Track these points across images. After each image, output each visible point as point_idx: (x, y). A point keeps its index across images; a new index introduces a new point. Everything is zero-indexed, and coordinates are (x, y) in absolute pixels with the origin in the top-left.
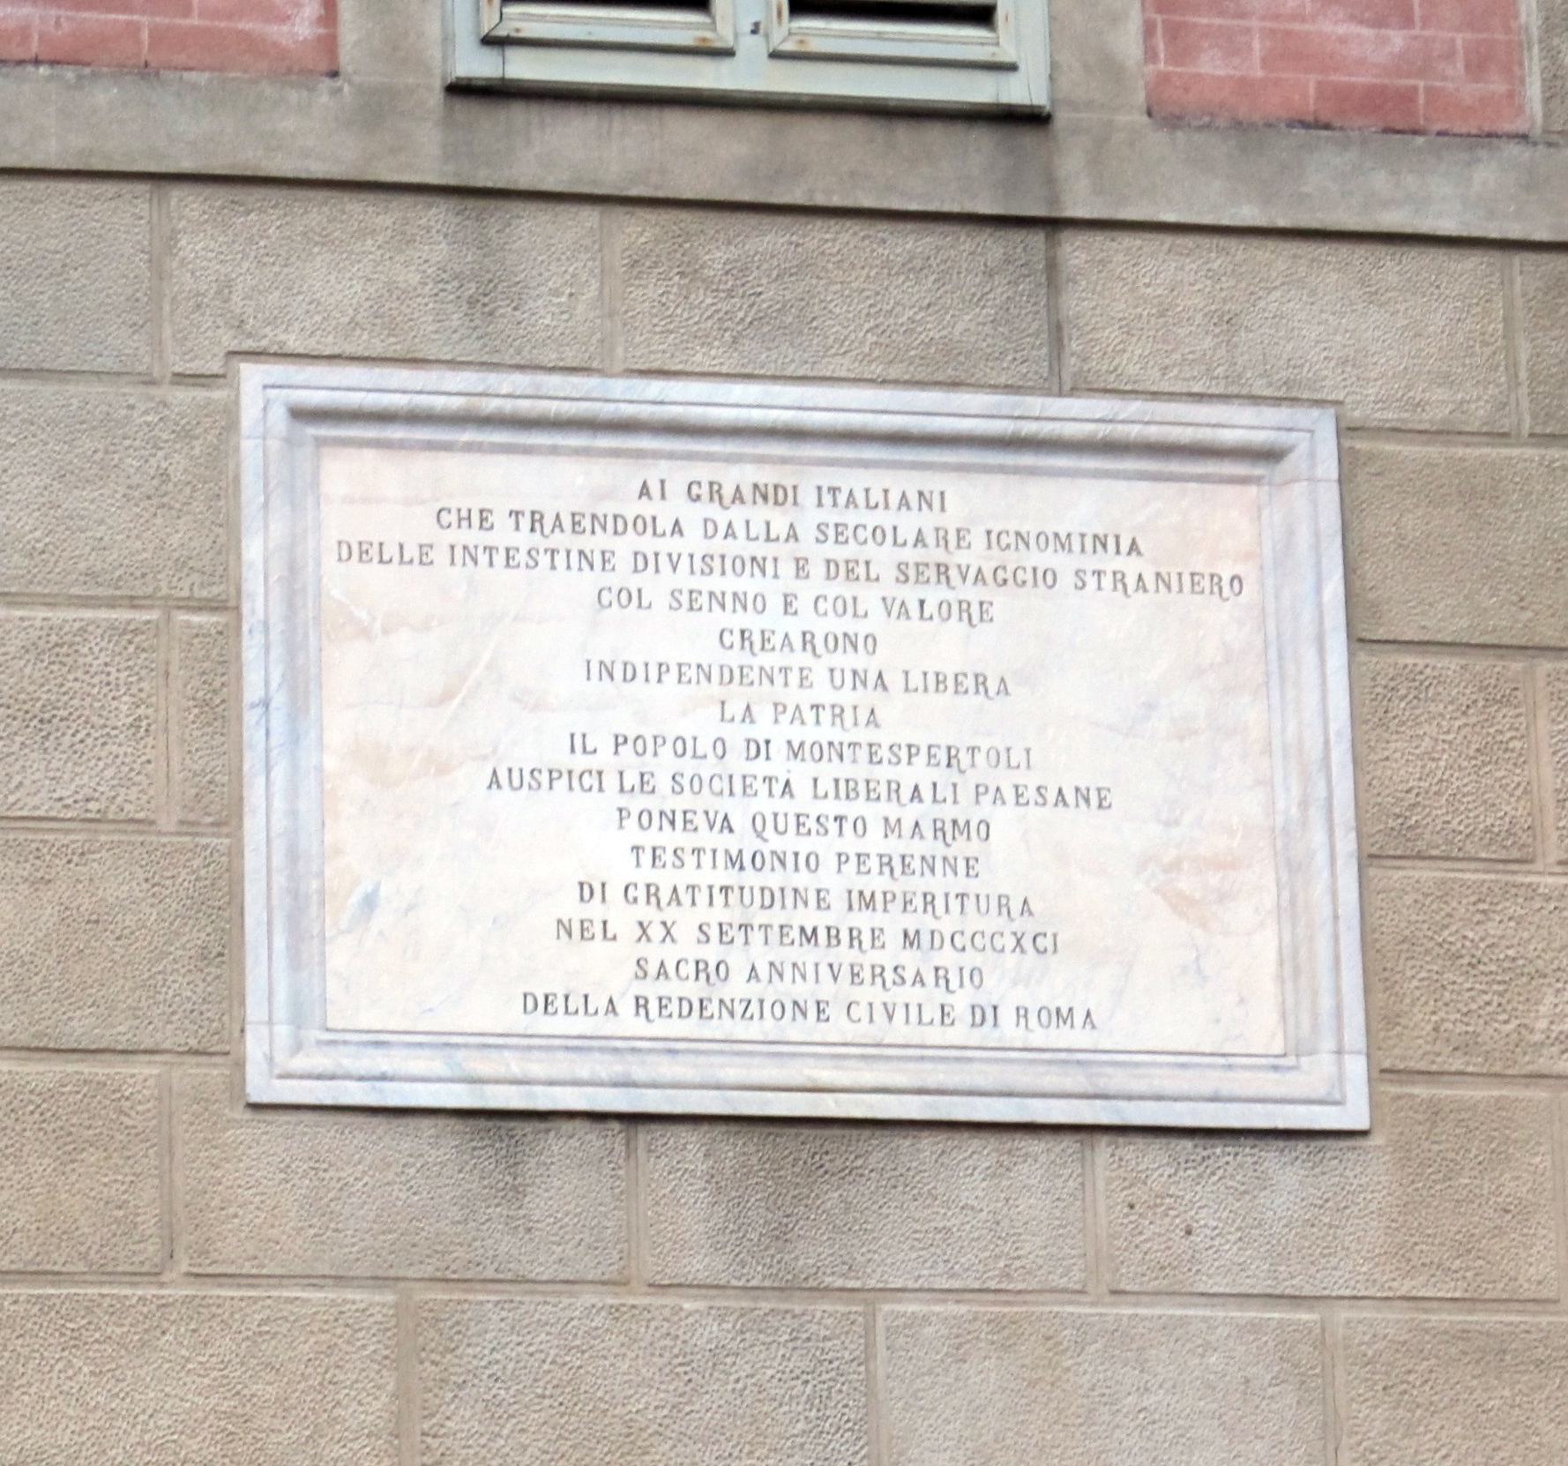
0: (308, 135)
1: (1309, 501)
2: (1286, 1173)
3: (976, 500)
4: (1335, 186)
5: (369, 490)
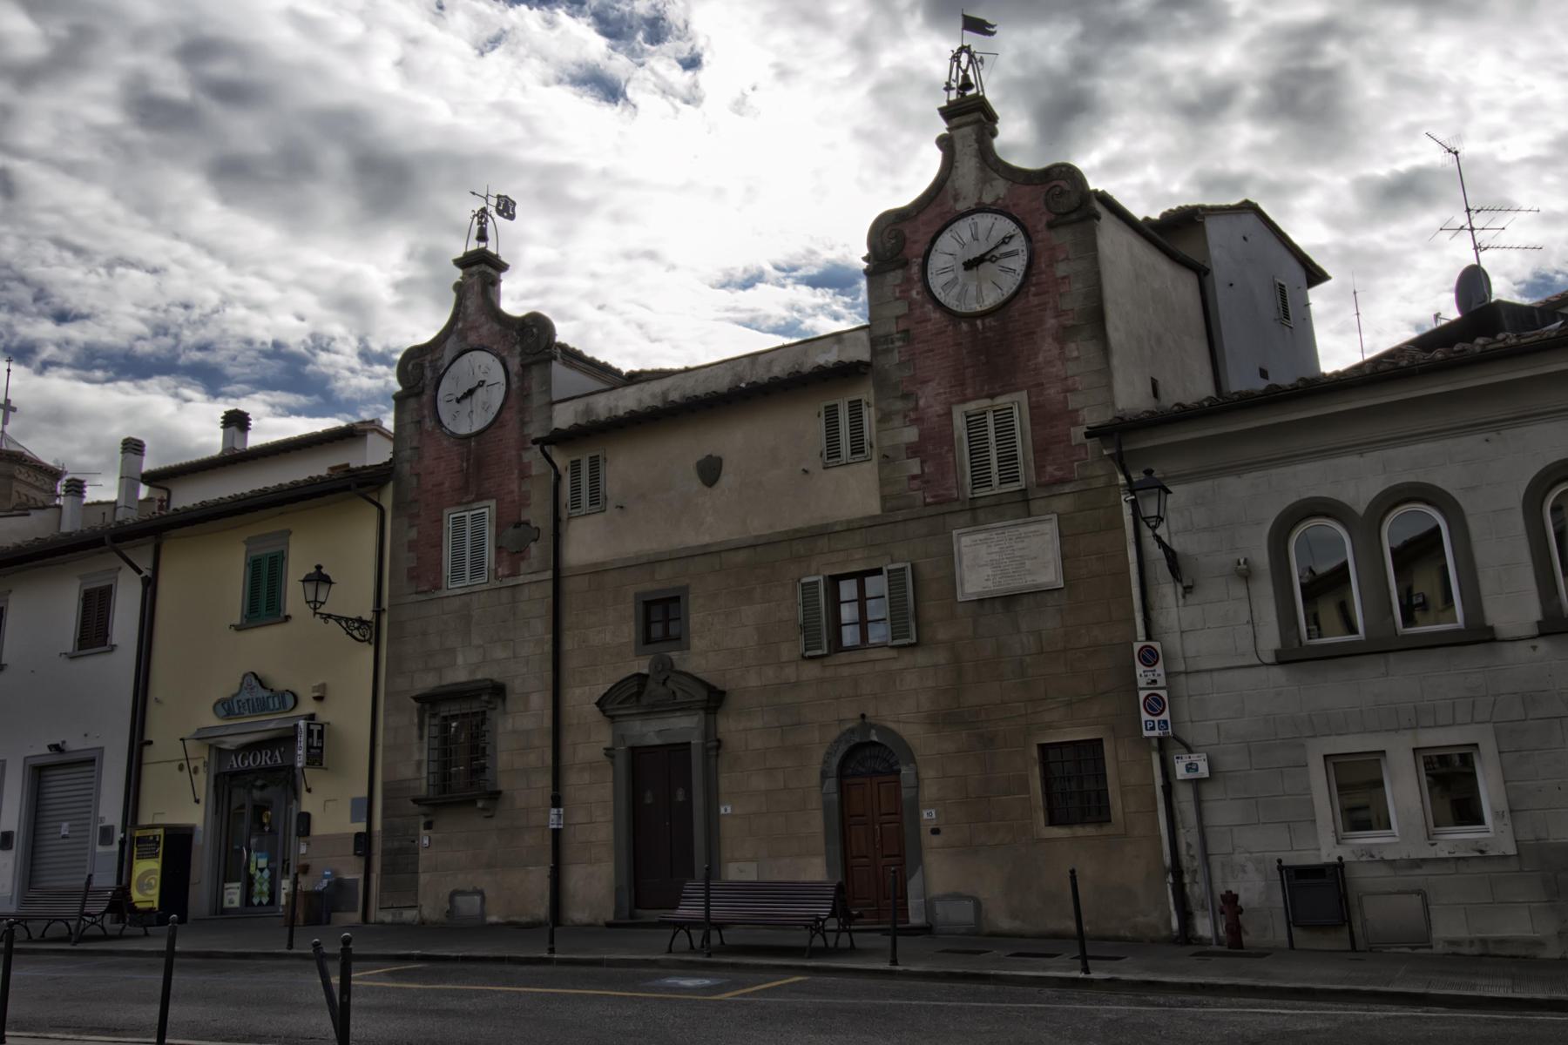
0: (956, 506)
1: (1055, 524)
2: (1056, 594)
3: (1022, 530)
4: (1056, 490)
5: (965, 540)
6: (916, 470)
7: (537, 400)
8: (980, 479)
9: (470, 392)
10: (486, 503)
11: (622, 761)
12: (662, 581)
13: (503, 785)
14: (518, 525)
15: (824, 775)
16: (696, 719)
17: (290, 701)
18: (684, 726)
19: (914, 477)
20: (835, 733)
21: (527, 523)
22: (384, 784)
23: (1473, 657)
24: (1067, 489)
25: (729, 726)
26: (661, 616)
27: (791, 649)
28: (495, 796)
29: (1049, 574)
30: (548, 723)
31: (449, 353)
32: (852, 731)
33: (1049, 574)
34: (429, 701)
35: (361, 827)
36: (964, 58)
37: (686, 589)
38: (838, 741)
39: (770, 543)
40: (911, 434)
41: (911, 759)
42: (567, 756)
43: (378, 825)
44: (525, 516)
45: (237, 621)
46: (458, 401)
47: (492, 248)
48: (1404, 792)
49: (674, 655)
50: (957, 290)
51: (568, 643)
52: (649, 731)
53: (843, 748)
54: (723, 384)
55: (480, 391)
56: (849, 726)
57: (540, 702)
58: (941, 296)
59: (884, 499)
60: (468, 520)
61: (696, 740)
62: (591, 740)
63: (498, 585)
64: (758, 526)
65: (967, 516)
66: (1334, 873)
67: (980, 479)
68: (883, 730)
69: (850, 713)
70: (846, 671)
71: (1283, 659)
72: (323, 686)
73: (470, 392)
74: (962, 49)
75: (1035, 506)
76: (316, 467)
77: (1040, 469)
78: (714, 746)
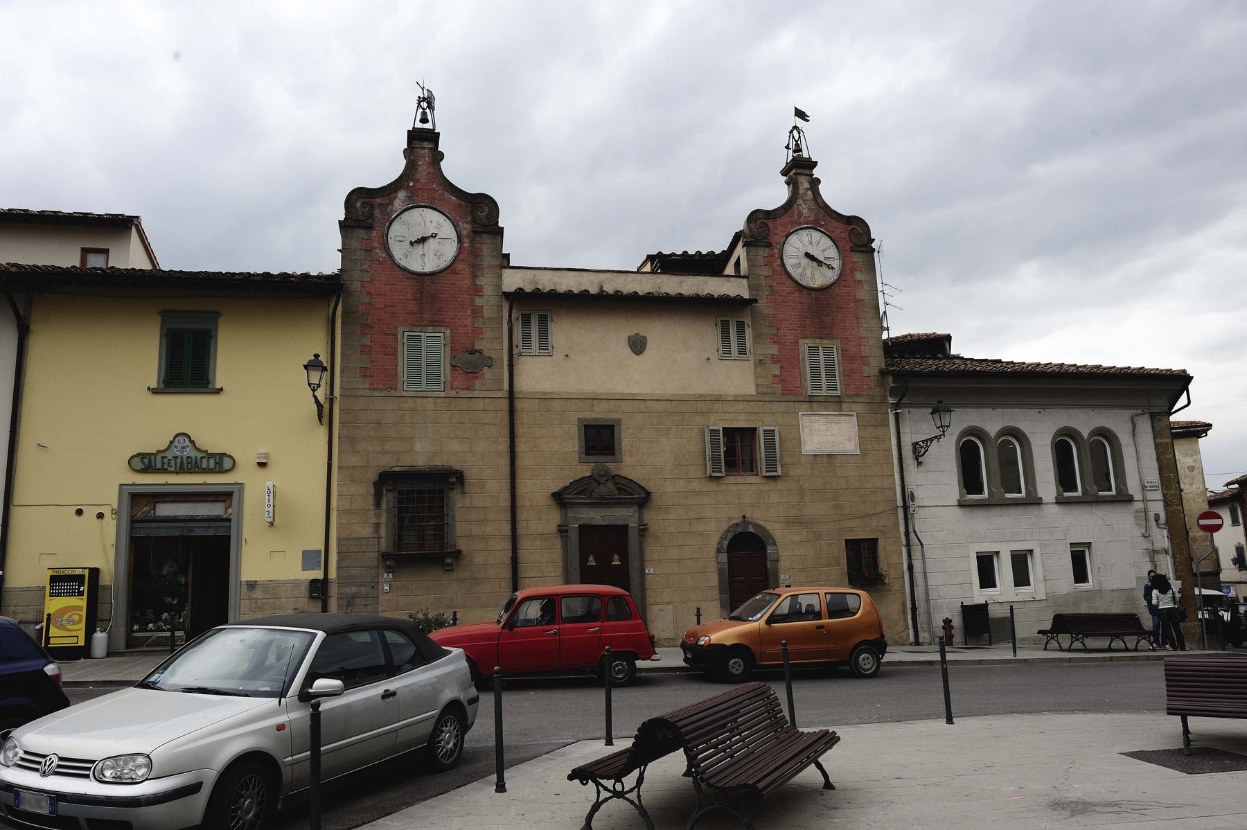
6: (778, 372)
7: (488, 261)
8: (816, 384)
9: (423, 240)
10: (443, 329)
11: (574, 536)
12: (599, 413)
13: (462, 545)
14: (473, 352)
15: (719, 551)
16: (632, 510)
17: (227, 463)
18: (623, 515)
19: (775, 376)
20: (725, 526)
21: (480, 352)
22: (339, 539)
23: (1032, 511)
24: (861, 399)
25: (651, 517)
26: (600, 438)
27: (695, 471)
28: (457, 554)
29: (851, 446)
30: (508, 504)
31: (398, 203)
32: (737, 525)
33: (851, 446)
34: (386, 480)
35: (318, 574)
36: (795, 132)
37: (619, 421)
38: (728, 531)
39: (701, 399)
40: (774, 350)
41: (774, 543)
42: (521, 527)
43: (333, 574)
44: (477, 346)
45: (154, 385)
46: (412, 243)
47: (805, 155)
48: (1004, 570)
49: (611, 466)
50: (800, 270)
51: (521, 447)
52: (597, 516)
53: (730, 536)
54: (591, 285)
55: (431, 241)
56: (735, 521)
57: (497, 488)
58: (792, 272)
59: (757, 386)
60: (424, 340)
61: (633, 524)
62: (541, 521)
63: (453, 393)
64: (672, 387)
65: (805, 406)
66: (983, 607)
67: (816, 384)
68: (757, 526)
69: (736, 516)
70: (733, 488)
71: (1058, 503)
72: (266, 455)
73: (423, 240)
74: (795, 127)
75: (844, 406)
76: (62, 255)
77: (847, 386)
78: (643, 530)
